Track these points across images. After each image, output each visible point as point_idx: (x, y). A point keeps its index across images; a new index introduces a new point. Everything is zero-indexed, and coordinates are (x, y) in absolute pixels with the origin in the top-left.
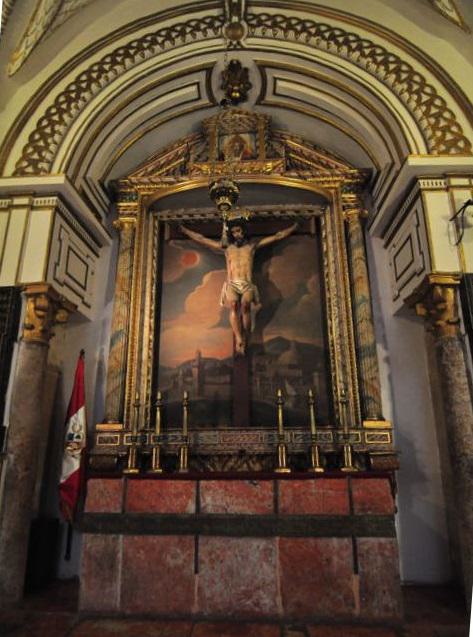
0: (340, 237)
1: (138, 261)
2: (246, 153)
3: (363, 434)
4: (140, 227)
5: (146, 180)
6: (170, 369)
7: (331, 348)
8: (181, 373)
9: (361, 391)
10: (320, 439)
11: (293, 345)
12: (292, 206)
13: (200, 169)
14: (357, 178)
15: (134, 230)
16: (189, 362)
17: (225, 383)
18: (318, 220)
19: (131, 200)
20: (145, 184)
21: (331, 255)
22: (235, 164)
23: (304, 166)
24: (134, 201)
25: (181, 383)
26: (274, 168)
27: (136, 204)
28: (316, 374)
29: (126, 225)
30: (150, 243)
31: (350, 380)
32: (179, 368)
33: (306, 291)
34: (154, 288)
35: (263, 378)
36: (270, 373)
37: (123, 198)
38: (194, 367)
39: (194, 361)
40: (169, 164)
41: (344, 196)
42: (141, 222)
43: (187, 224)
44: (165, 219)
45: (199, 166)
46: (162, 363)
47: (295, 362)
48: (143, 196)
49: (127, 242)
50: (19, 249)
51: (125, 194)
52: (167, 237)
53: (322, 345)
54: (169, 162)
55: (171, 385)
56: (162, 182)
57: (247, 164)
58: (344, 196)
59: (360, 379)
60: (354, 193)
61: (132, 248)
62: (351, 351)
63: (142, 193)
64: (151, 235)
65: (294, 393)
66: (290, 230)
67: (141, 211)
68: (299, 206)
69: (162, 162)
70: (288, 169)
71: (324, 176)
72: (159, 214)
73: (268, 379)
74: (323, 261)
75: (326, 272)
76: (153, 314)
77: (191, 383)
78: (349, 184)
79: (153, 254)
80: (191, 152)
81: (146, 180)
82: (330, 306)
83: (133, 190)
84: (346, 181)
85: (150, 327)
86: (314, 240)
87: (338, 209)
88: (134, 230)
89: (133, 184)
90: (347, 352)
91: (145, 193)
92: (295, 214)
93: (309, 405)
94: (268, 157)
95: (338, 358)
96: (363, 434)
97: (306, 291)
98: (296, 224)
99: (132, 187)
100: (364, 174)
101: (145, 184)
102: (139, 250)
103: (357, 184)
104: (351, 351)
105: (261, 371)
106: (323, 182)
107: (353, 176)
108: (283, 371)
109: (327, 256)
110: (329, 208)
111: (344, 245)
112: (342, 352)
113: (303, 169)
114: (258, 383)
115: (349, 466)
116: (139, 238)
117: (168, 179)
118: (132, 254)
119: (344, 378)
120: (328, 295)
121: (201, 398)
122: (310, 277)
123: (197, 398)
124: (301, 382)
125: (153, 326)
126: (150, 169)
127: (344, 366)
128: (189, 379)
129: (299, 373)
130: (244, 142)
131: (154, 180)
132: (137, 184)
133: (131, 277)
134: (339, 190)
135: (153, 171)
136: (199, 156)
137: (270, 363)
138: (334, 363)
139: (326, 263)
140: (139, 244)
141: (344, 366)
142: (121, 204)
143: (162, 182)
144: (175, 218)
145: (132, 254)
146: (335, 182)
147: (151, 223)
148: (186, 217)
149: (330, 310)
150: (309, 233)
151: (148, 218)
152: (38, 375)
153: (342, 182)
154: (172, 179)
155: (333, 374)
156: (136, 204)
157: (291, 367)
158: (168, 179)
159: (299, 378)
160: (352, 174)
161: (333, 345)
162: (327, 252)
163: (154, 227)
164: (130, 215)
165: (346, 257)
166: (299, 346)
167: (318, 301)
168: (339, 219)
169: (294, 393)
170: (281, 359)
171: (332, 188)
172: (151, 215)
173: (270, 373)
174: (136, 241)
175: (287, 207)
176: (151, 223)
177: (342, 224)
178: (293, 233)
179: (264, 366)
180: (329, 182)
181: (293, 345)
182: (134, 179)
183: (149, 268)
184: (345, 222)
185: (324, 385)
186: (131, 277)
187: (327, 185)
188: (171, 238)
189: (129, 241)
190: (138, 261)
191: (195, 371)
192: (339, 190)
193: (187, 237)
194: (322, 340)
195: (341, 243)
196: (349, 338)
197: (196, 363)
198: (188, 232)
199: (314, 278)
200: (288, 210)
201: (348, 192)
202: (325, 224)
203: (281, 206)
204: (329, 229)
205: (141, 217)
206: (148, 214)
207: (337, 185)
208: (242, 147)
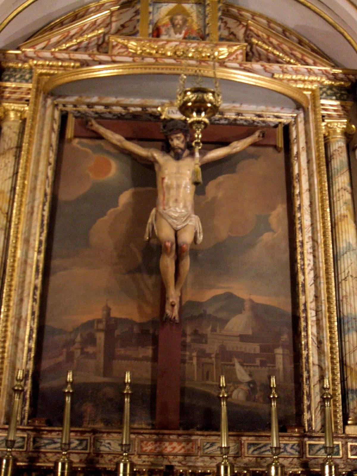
0: (318, 158)
1: (26, 168)
2: (190, 29)
3: (345, 445)
4: (33, 119)
5: (47, 54)
6: (62, 332)
7: (303, 315)
8: (79, 339)
9: (343, 380)
10: (285, 450)
11: (247, 306)
12: (253, 107)
13: (126, 47)
14: (342, 80)
15: (24, 121)
16: (90, 324)
17: (145, 359)
18: (287, 129)
19: (22, 79)
20: (45, 59)
21: (304, 179)
22: (174, 44)
23: (271, 55)
24: (27, 81)
25: (78, 354)
26: (230, 54)
27: (30, 86)
28: (279, 351)
29: (12, 115)
30: (45, 142)
31: (327, 363)
32: (77, 330)
33: (268, 228)
34: (47, 208)
35: (202, 354)
36: (212, 348)
37: (11, 76)
38: (98, 330)
39: (99, 321)
40: (81, 35)
41: (323, 101)
42: (35, 112)
43: (100, 117)
44: (70, 108)
45: (126, 42)
46: (50, 323)
47: (250, 332)
48: (41, 74)
49: (10, 139)
50: (6, 27)
51: (15, 70)
52: (69, 133)
53: (288, 309)
54: (82, 32)
55: (62, 358)
56: (70, 60)
57: (193, 46)
58: (323, 101)
59: (343, 363)
60: (337, 99)
61: (19, 147)
62: (330, 322)
63: (40, 71)
64: (46, 132)
65: (247, 379)
66: (249, 141)
67: (36, 97)
68: (260, 109)
69: (73, 32)
70: (248, 57)
71: (297, 72)
72: (61, 100)
73: (209, 356)
74: (294, 187)
75: (298, 203)
76: (43, 247)
77: (94, 356)
78: (331, 87)
79: (48, 158)
80: (114, 19)
81: (47, 54)
82: (302, 253)
83: (26, 66)
84: (327, 82)
85: (37, 267)
86: (281, 156)
87: (316, 119)
88: (24, 121)
89: (26, 58)
90: (325, 323)
91: (44, 71)
92: (255, 118)
93: (270, 400)
94: (221, 39)
95: (312, 330)
96: (345, 445)
97: (268, 228)
98: (257, 134)
99: (25, 62)
100: (351, 77)
101: (45, 59)
102: (28, 152)
103: (340, 88)
104: (330, 322)
105: (200, 342)
106: (296, 81)
107: (335, 77)
108: (234, 345)
109: (299, 181)
110: (302, 115)
111: (324, 168)
112: (318, 322)
113: (269, 60)
114: (195, 361)
115: (7, 426)
116: (31, 136)
117: (78, 56)
118: (18, 157)
119: (320, 360)
120: (299, 238)
121: (106, 380)
122: (274, 208)
123: (101, 379)
124: (258, 362)
125: (41, 266)
126: (54, 40)
127: (320, 343)
128: (90, 350)
129: (254, 348)
130: (188, 15)
131: (59, 55)
132: (33, 59)
133: (13, 189)
134: (318, 93)
135: (58, 43)
136: (123, 26)
137: (214, 330)
138: (307, 336)
139: (297, 191)
140: (30, 143)
141: (320, 343)
142: (8, 84)
143: (70, 60)
144: (83, 108)
145: (18, 157)
146: (312, 82)
147: (49, 112)
148: (100, 108)
149: (303, 259)
150: (275, 147)
151: (44, 106)
152: (105, 312)
153: (321, 83)
154: (85, 57)
155: (304, 353)
156: (30, 86)
157: (243, 338)
158: (78, 56)
159: (256, 355)
160: (334, 74)
161: (305, 310)
162: (299, 175)
163: (53, 119)
164: (20, 100)
165: (11, 249)
166: (255, 306)
167: (285, 244)
168: (317, 134)
169: (247, 379)
170: (229, 326)
171: (308, 90)
172: (49, 101)
173: (212, 348)
174: (26, 137)
175: (245, 107)
176: (49, 112)
177: (322, 139)
178: (254, 144)
179: (204, 336)
180: (304, 81)
181: (247, 306)
182: (29, 51)
183: (41, 177)
184: (325, 137)
185: (290, 367)
186: (13, 189)
187: (301, 86)
188: (75, 137)
189: (15, 138)
190: (26, 168)
191: (101, 337)
192: (318, 93)
193: (99, 137)
194: (289, 300)
195: (319, 166)
196: (329, 302)
197: (101, 326)
198: (102, 130)
199: (281, 209)
200: (247, 112)
201: (328, 97)
202: (297, 136)
203: (237, 105)
204: (302, 144)
205: (36, 104)
206: (45, 100)
207: (314, 86)
208: (185, 21)
